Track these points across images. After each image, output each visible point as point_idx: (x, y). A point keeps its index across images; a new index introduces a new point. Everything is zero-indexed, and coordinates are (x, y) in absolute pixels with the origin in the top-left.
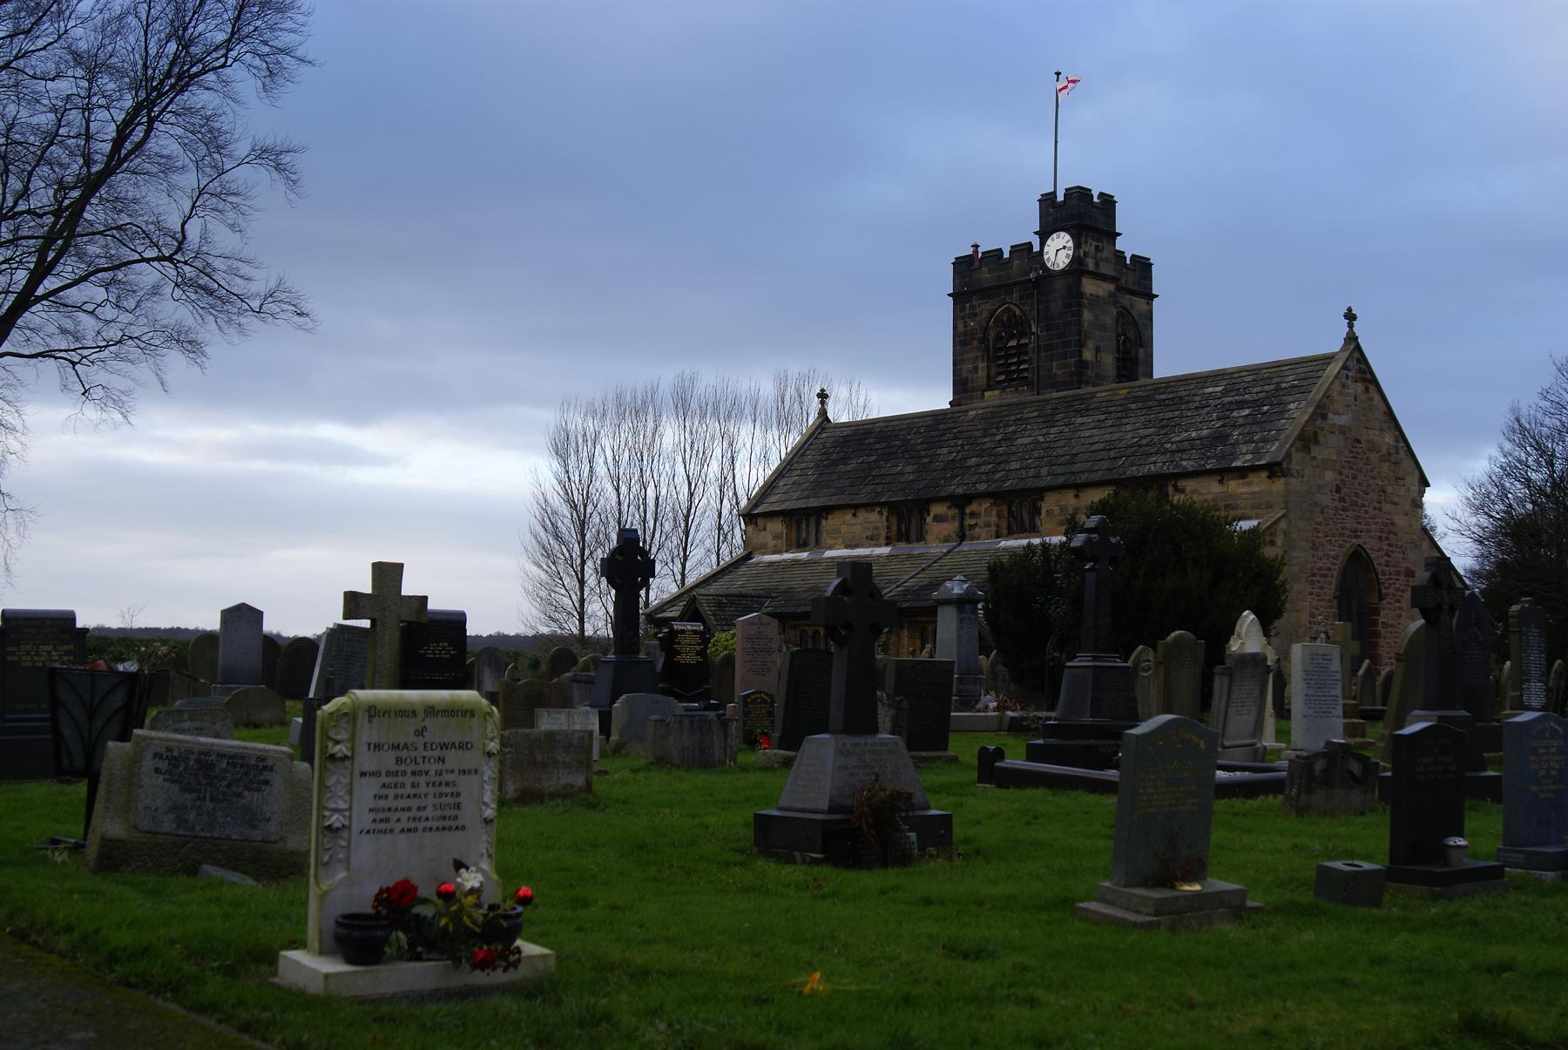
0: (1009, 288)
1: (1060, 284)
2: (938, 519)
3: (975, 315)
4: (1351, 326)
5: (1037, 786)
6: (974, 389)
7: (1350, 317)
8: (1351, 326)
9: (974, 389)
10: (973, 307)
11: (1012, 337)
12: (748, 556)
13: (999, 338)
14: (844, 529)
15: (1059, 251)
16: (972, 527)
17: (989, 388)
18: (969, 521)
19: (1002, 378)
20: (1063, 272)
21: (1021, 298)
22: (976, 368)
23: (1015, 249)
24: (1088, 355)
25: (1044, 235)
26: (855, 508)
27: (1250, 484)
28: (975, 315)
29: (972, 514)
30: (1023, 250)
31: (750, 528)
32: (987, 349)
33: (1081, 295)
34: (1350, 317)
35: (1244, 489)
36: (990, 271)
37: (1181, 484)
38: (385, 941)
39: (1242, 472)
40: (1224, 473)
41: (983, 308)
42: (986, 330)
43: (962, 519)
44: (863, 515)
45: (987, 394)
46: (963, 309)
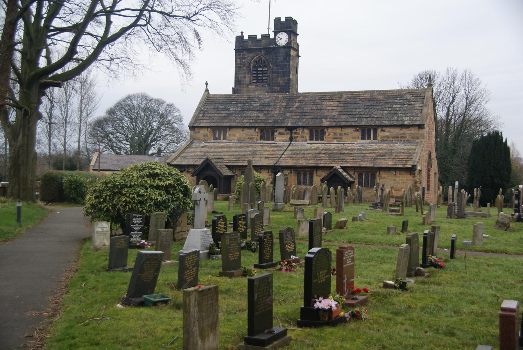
0: (260, 50)
1: (282, 51)
2: (280, 133)
3: (245, 58)
4: (207, 86)
5: (390, 288)
6: (244, 84)
7: (207, 84)
8: (207, 86)
9: (244, 84)
10: (244, 55)
11: (260, 67)
12: (192, 143)
13: (254, 67)
14: (237, 135)
15: (283, 39)
16: (295, 137)
17: (250, 84)
18: (294, 136)
19: (255, 81)
20: (284, 47)
21: (265, 54)
22: (245, 77)
23: (263, 36)
24: (291, 76)
25: (276, 33)
26: (243, 127)
27: (411, 130)
28: (245, 58)
29: (296, 133)
30: (266, 37)
31: (192, 131)
32: (250, 70)
33: (290, 55)
34: (207, 84)
35: (409, 132)
36: (252, 42)
37: (384, 129)
38: (6, 109)
39: (408, 126)
40: (402, 126)
41: (249, 56)
42: (250, 64)
43: (291, 134)
44: (246, 131)
45: (249, 86)
46: (240, 55)
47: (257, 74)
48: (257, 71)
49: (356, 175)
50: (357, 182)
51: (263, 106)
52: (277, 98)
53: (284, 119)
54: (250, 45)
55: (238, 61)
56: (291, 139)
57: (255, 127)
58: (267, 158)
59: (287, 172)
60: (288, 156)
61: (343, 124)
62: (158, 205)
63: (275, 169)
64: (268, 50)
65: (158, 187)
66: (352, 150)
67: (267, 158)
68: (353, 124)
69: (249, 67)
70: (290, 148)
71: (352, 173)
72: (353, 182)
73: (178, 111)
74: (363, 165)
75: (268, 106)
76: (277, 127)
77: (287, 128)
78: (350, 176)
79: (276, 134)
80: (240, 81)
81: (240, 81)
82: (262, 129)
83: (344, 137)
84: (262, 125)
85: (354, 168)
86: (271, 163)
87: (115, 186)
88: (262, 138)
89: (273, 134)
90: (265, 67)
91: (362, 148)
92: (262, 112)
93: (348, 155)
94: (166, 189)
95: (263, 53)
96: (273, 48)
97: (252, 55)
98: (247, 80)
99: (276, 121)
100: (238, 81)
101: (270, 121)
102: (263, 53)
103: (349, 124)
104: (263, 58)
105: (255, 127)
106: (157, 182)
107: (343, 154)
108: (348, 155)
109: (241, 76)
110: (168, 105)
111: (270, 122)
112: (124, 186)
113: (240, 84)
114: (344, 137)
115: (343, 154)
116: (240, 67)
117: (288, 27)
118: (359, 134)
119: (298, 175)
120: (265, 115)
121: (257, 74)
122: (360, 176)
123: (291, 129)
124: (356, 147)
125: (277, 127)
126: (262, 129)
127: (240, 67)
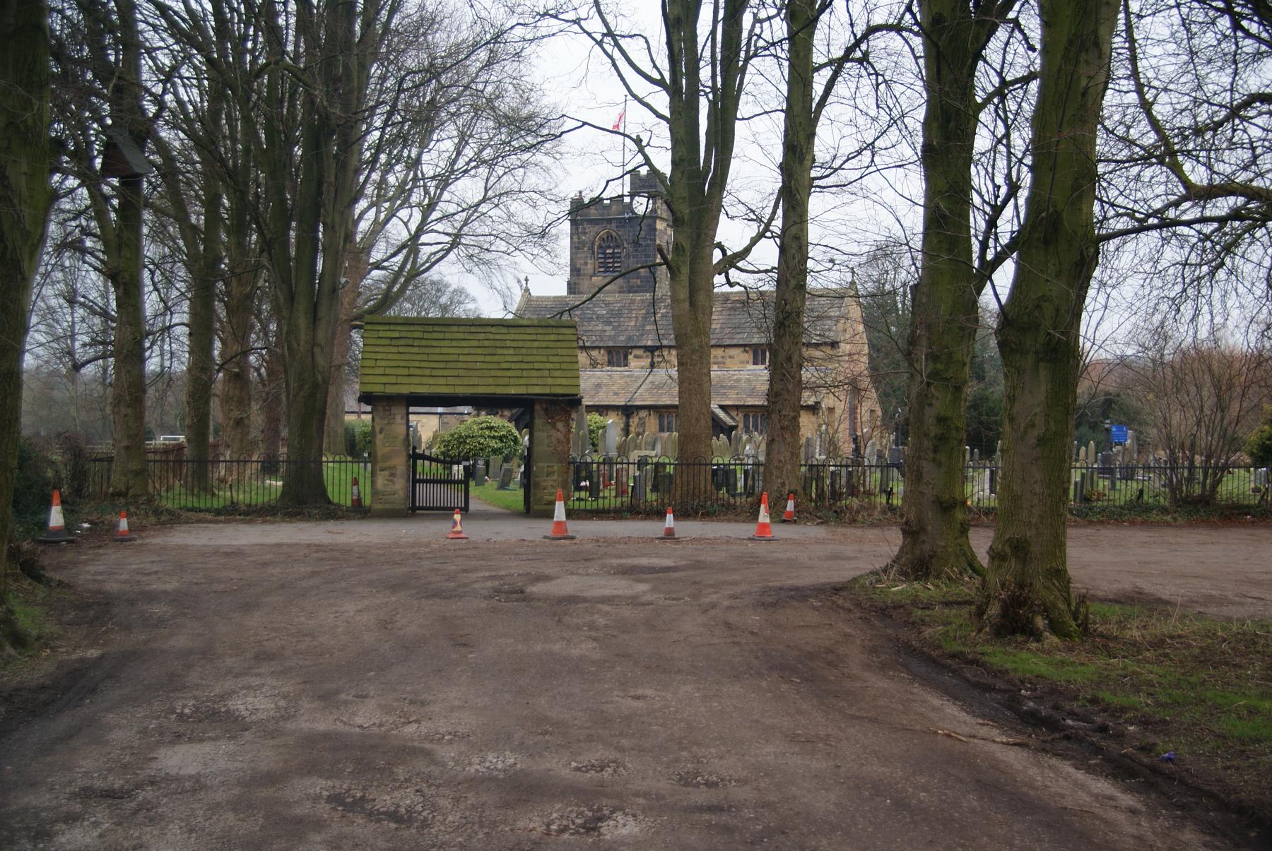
0: (610, 221)
2: (636, 357)
11: (609, 247)
13: (600, 247)
17: (594, 275)
18: (656, 359)
22: (586, 263)
41: (591, 230)
47: (605, 258)
48: (604, 253)
49: (740, 417)
50: (741, 425)
51: (612, 314)
52: (633, 302)
53: (642, 335)
54: (593, 213)
55: (576, 240)
56: (652, 365)
57: (599, 348)
58: (616, 394)
59: (643, 414)
60: (646, 390)
61: (728, 342)
62: (495, 451)
63: (627, 411)
64: (622, 222)
65: (494, 437)
66: (738, 381)
67: (616, 394)
68: (741, 342)
69: (592, 248)
70: (650, 378)
71: (734, 413)
72: (735, 428)
73: (474, 300)
74: (750, 402)
75: (619, 314)
76: (632, 347)
77: (646, 348)
78: (732, 418)
79: (630, 357)
80: (579, 270)
81: (579, 270)
82: (610, 350)
83: (728, 361)
84: (611, 344)
85: (737, 407)
86: (621, 401)
87: (460, 437)
88: (610, 363)
89: (626, 358)
90: (618, 247)
91: (752, 378)
92: (610, 323)
93: (732, 387)
94: (501, 438)
95: (614, 225)
96: (630, 219)
97: (596, 228)
98: (590, 268)
99: (630, 338)
100: (575, 271)
101: (622, 338)
102: (614, 225)
103: (734, 342)
104: (614, 234)
105: (599, 348)
106: (493, 433)
107: (724, 387)
108: (732, 387)
109: (579, 263)
110: (455, 291)
111: (622, 340)
112: (468, 437)
113: (579, 275)
114: (728, 361)
115: (724, 387)
116: (578, 248)
117: (651, 187)
118: (749, 356)
119: (661, 418)
120: (615, 328)
121: (605, 258)
122: (746, 417)
123: (651, 350)
124: (744, 375)
125: (632, 347)
126: (610, 350)
127: (578, 248)
